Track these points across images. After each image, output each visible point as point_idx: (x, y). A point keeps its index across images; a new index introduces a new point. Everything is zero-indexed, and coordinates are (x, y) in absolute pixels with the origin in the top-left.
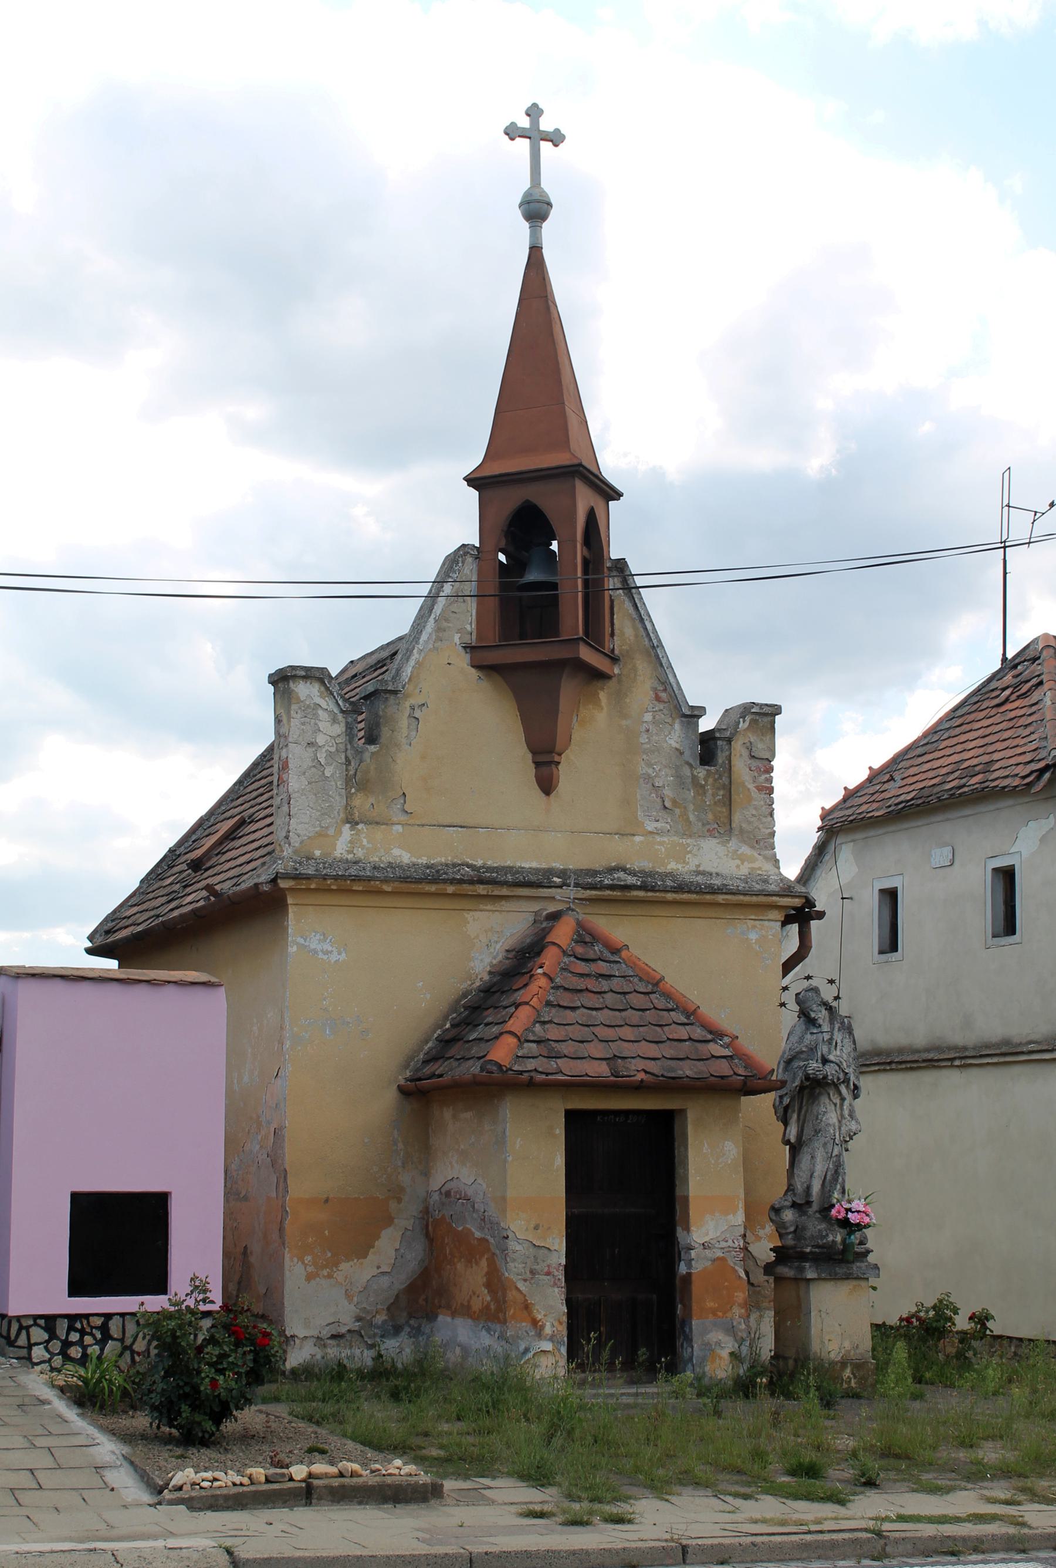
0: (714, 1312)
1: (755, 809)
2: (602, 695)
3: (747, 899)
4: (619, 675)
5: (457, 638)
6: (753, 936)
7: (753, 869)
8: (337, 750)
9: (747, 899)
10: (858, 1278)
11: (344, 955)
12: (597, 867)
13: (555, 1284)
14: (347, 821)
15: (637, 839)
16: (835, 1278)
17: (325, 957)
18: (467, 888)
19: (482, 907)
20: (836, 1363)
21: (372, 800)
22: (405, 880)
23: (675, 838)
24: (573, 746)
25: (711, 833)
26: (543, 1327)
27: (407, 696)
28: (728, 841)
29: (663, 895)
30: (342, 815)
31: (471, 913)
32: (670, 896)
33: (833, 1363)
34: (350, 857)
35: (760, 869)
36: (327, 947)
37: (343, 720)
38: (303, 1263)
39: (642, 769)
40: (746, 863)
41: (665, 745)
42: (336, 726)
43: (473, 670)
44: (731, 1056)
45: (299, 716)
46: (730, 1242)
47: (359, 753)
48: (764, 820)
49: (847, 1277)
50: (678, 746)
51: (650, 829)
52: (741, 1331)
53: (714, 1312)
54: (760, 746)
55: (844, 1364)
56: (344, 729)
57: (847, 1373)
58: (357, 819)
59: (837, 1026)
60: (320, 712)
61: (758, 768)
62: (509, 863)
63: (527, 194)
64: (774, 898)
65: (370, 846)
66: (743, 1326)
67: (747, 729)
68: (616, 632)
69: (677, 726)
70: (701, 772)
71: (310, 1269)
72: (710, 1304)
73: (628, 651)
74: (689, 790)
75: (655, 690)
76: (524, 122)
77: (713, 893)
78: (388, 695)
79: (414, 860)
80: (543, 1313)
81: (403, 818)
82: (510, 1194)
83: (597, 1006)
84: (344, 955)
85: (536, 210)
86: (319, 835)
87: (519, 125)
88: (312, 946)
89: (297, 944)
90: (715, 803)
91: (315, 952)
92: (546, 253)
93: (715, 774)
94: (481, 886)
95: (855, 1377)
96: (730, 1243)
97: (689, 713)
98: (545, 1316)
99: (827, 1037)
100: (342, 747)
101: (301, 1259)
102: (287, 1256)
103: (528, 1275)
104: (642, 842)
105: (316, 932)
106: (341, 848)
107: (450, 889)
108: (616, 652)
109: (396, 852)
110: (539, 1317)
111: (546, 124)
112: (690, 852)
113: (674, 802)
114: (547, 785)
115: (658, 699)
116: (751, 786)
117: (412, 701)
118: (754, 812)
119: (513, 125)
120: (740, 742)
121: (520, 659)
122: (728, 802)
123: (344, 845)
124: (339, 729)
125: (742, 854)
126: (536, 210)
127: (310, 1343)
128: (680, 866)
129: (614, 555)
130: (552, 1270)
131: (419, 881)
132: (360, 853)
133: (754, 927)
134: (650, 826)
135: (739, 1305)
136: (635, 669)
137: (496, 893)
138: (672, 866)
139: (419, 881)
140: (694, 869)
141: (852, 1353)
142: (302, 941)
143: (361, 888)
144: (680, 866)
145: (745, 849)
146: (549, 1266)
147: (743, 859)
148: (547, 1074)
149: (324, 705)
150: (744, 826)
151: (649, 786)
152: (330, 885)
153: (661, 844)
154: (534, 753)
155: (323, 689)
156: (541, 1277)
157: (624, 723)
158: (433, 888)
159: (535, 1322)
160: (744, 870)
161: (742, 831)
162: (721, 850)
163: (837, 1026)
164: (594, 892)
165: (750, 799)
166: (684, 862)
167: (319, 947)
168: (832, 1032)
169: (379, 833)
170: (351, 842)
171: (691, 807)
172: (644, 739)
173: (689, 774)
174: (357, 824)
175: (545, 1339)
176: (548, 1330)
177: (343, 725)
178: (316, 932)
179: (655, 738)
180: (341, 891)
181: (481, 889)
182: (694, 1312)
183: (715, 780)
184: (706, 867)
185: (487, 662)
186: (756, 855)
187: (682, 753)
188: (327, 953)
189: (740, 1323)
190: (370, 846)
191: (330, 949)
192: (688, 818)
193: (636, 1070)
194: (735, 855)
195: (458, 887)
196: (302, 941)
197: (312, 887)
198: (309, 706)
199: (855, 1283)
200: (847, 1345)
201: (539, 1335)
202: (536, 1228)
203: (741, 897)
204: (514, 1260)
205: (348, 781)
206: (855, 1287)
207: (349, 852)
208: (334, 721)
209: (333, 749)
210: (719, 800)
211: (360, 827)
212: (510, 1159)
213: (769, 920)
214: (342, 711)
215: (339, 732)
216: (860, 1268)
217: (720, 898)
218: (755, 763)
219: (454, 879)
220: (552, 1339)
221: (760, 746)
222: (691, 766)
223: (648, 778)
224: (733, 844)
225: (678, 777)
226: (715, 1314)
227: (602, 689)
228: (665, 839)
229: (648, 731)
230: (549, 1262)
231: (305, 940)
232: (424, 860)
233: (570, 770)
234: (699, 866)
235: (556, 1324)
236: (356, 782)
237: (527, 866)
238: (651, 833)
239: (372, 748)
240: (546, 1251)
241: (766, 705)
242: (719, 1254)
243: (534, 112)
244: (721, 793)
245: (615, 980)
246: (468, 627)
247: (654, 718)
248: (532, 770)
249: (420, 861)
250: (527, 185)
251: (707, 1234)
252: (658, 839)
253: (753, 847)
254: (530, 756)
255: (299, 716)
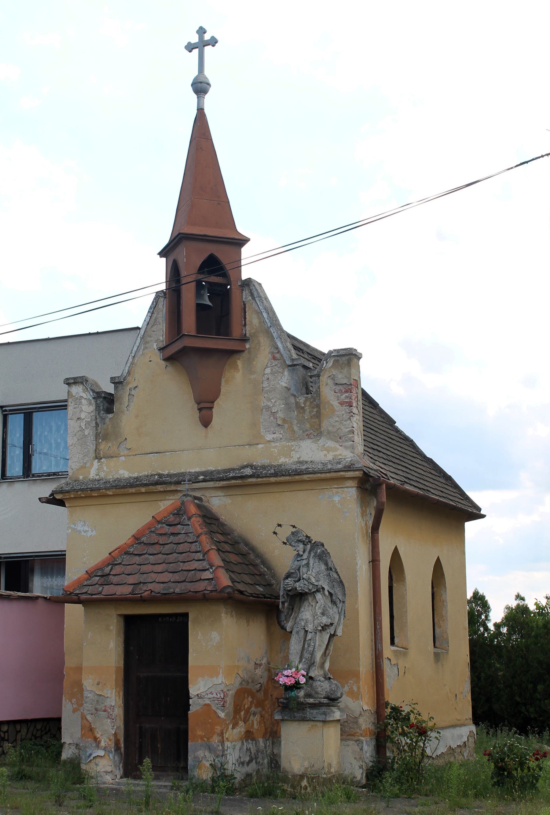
0: (202, 738)
1: (338, 417)
2: (239, 363)
3: (323, 476)
4: (249, 348)
5: (155, 347)
6: (336, 499)
7: (335, 455)
8: (91, 420)
9: (323, 476)
10: (310, 720)
11: (94, 532)
12: (235, 466)
13: (108, 717)
14: (96, 458)
15: (260, 446)
16: (294, 719)
17: (85, 534)
18: (152, 488)
19: (167, 498)
20: (297, 775)
21: (110, 444)
22: (116, 487)
23: (284, 443)
24: (221, 396)
25: (309, 436)
26: (100, 742)
27: (128, 383)
28: (318, 440)
29: (267, 479)
30: (94, 455)
31: (163, 502)
32: (273, 479)
33: (294, 776)
34: (97, 477)
35: (340, 455)
36: (86, 528)
37: (95, 403)
38: (71, 703)
39: (264, 402)
40: (331, 452)
41: (278, 386)
42: (91, 407)
43: (163, 362)
44: (212, 579)
45: (73, 404)
46: (215, 694)
47: (103, 419)
48: (345, 423)
49: (304, 720)
50: (286, 385)
51: (268, 439)
52: (219, 750)
53: (202, 738)
54: (340, 376)
55: (302, 777)
56: (94, 408)
57: (304, 783)
58: (102, 456)
59: (312, 554)
60: (83, 401)
61: (341, 391)
62: (183, 471)
63: (196, 78)
64: (342, 473)
65: (108, 470)
66: (220, 748)
67: (332, 367)
68: (247, 323)
69: (286, 373)
70: (301, 400)
71: (75, 706)
72: (199, 733)
73: (254, 333)
74: (294, 411)
75: (273, 353)
76: (207, 37)
77: (298, 474)
78: (118, 385)
79: (131, 475)
80: (100, 733)
81: (126, 452)
82: (85, 664)
83: (155, 552)
84: (94, 532)
85: (200, 87)
86: (82, 467)
87: (192, 42)
88: (79, 529)
89: (71, 528)
90: (311, 417)
91: (80, 531)
92: (206, 111)
93: (311, 399)
94: (160, 486)
95: (310, 786)
96: (215, 695)
97: (290, 364)
98: (101, 735)
99: (305, 562)
100: (94, 418)
101: (70, 701)
102: (64, 698)
103: (94, 711)
104: (263, 448)
105: (81, 521)
106: (92, 474)
107: (143, 490)
108: (247, 335)
109: (121, 472)
110: (98, 736)
111: (195, 39)
112: (294, 450)
113: (284, 420)
114: (206, 422)
115: (274, 358)
116: (335, 403)
117: (130, 386)
118: (337, 419)
119: (189, 43)
120: (326, 376)
121: (220, 347)
122: (318, 415)
123: (95, 471)
124: (92, 408)
125: (328, 447)
126: (200, 87)
127: (73, 747)
128: (287, 460)
129: (244, 277)
130: (107, 709)
131: (124, 487)
132: (102, 475)
133: (337, 492)
134: (269, 437)
135: (218, 734)
136: (259, 343)
137: (168, 489)
138: (282, 460)
139: (124, 487)
140: (297, 460)
141: (309, 769)
142: (73, 526)
143: (96, 495)
144: (287, 460)
145: (330, 444)
146: (105, 706)
147: (328, 450)
148: (92, 595)
149: (84, 396)
150: (330, 429)
151: (269, 413)
152: (80, 495)
153: (275, 447)
154: (198, 403)
155: (84, 388)
156: (101, 713)
157: (253, 377)
158: (133, 490)
159: (95, 739)
160: (330, 457)
161: (329, 432)
162: (314, 446)
163: (312, 554)
164: (225, 482)
165: (333, 410)
166: (290, 457)
167: (82, 529)
168: (308, 558)
169: (112, 462)
170: (98, 469)
171: (295, 421)
172: (265, 384)
173: (294, 401)
174: (101, 459)
175: (101, 749)
176: (103, 744)
177: (94, 405)
178: (81, 521)
179: (272, 383)
180: (86, 497)
181: (160, 488)
182: (189, 737)
183: (311, 403)
184: (304, 458)
185: (176, 356)
186: (338, 446)
187: (289, 389)
188: (86, 531)
189: (218, 746)
190: (108, 470)
191: (87, 529)
192: (293, 430)
193: (144, 591)
194: (324, 448)
195: (147, 488)
196: (73, 526)
197: (72, 496)
198: (77, 398)
199: (312, 723)
200: (306, 764)
201: (98, 746)
202: (98, 684)
203: (319, 475)
204: (86, 703)
205: (97, 436)
206: (312, 726)
207: (97, 475)
208: (90, 404)
209: (89, 420)
210: (314, 415)
211: (102, 460)
212: (85, 644)
213: (347, 487)
214: (93, 398)
215: (92, 410)
216: (312, 713)
217: (305, 477)
218: (338, 388)
219: (143, 484)
220: (105, 749)
221: (340, 376)
222: (294, 396)
223: (268, 408)
224: (322, 441)
225: (287, 404)
226: (202, 739)
227: (239, 359)
228: (278, 444)
229: (268, 379)
230: (106, 704)
231: (75, 526)
232: (136, 475)
233: (221, 411)
234: (300, 458)
235: (108, 740)
236: (101, 436)
237: (193, 471)
238: (269, 441)
239: (110, 416)
240: (104, 698)
241: (342, 349)
242: (208, 702)
243: (201, 31)
244: (315, 410)
245: (180, 536)
246: (161, 338)
247: (272, 370)
248: (197, 414)
249: (134, 475)
250: (196, 73)
251: (199, 689)
252: (273, 444)
253: (337, 442)
254: (196, 406)
255: (73, 404)
